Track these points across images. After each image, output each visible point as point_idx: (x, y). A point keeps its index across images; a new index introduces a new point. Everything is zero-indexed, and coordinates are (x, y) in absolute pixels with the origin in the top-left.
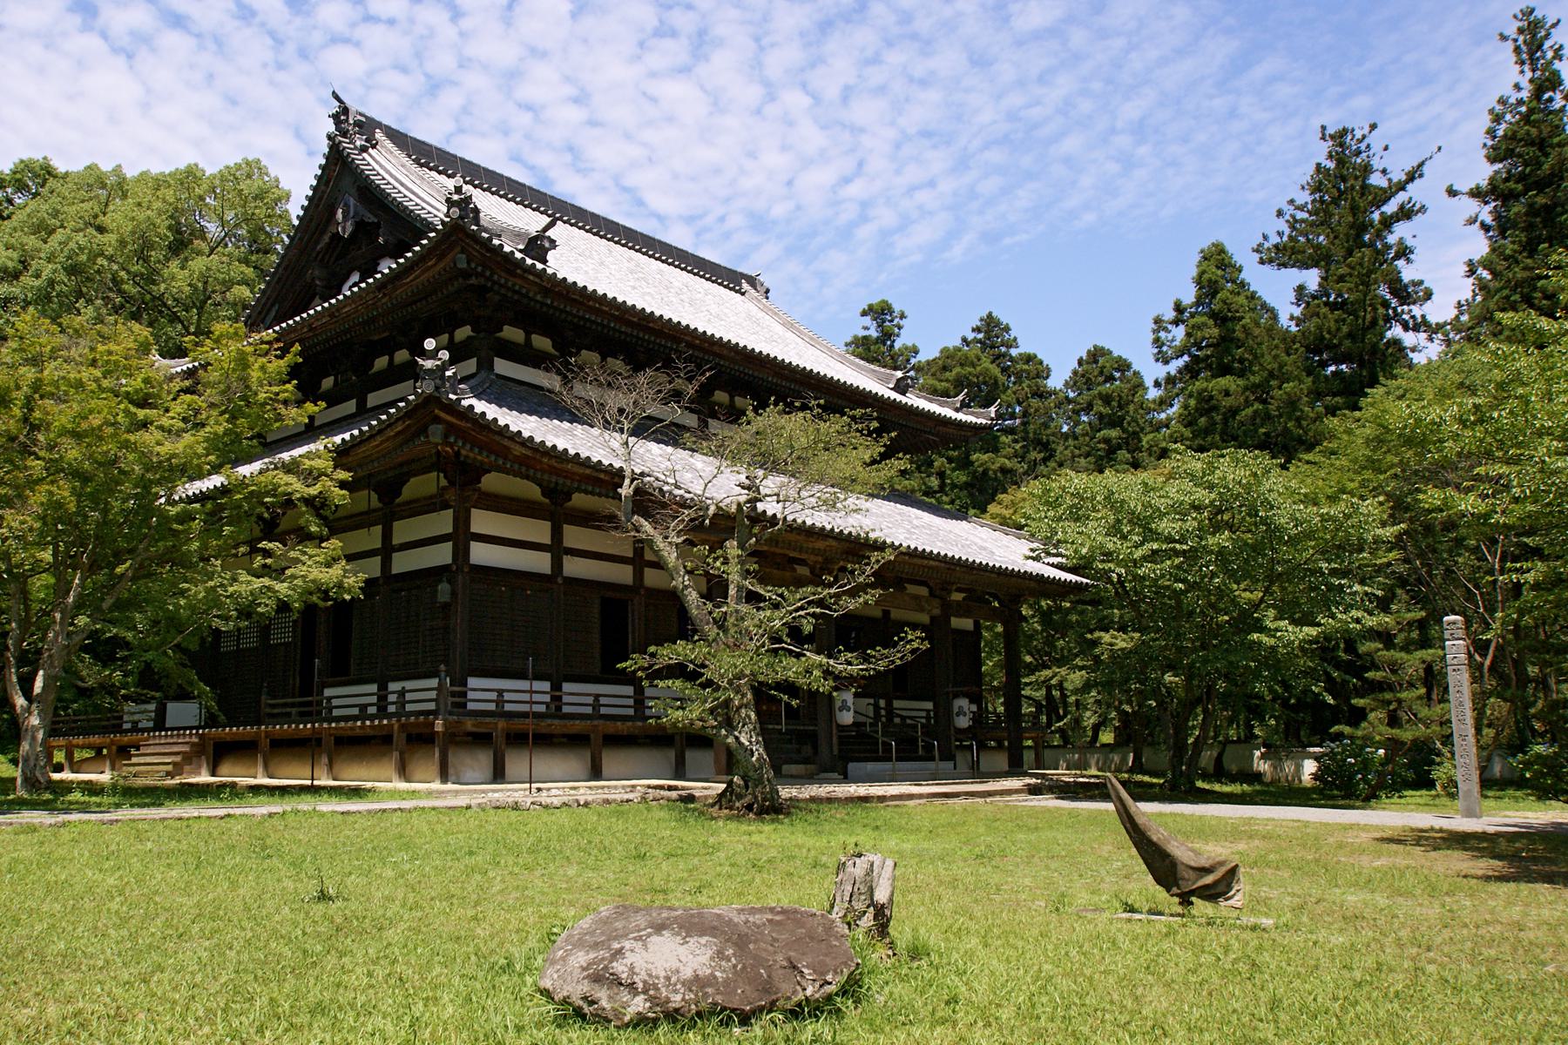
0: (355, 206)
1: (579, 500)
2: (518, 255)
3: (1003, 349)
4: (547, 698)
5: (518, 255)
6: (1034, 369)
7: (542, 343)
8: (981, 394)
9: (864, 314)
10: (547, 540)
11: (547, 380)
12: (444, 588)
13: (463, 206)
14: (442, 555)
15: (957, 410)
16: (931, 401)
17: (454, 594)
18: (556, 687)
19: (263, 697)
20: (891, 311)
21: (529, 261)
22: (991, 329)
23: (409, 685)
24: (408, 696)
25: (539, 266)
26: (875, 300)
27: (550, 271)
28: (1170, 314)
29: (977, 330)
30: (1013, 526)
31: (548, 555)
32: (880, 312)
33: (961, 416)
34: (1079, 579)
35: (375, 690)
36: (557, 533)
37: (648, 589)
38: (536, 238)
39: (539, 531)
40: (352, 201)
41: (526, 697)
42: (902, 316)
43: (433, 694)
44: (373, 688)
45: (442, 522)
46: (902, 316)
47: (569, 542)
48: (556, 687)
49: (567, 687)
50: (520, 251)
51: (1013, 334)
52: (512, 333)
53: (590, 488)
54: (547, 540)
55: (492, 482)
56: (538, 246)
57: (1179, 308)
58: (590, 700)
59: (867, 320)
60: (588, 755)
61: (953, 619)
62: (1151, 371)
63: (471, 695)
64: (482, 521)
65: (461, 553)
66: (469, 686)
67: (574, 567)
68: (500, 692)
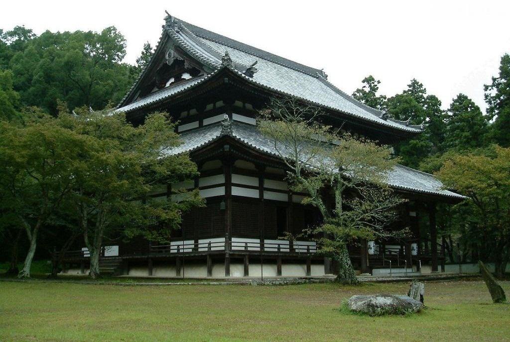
0: (174, 54)
1: (269, 169)
2: (243, 75)
3: (420, 94)
4: (193, 246)
5: (243, 75)
6: (434, 101)
7: (249, 106)
8: (416, 118)
9: (364, 82)
10: (257, 185)
11: (251, 121)
12: (223, 204)
13: (227, 59)
14: (221, 192)
15: (407, 126)
16: (396, 122)
17: (226, 207)
18: (196, 242)
19: (150, 245)
20: (373, 79)
21: (247, 77)
22: (415, 86)
23: (212, 240)
24: (212, 245)
25: (251, 79)
26: (367, 77)
27: (254, 81)
28: (490, 83)
29: (410, 86)
30: (430, 172)
31: (258, 191)
32: (369, 80)
33: (409, 129)
34: (461, 196)
35: (193, 243)
36: (261, 183)
37: (294, 203)
38: (250, 69)
39: (255, 182)
40: (172, 52)
41: (185, 247)
42: (379, 82)
43: (223, 244)
44: (399, 247)
45: (221, 179)
46: (379, 82)
47: (265, 186)
48: (196, 242)
49: (266, 241)
50: (244, 73)
51: (424, 87)
52: (239, 104)
53: (278, 166)
54: (257, 185)
55: (239, 164)
56: (250, 71)
57: (494, 80)
58: (176, 247)
59: (366, 84)
60: (305, 267)
61: (415, 216)
62: (484, 107)
63: (233, 244)
64: (235, 179)
65: (228, 191)
66: (199, 243)
67: (268, 196)
68: (246, 243)
